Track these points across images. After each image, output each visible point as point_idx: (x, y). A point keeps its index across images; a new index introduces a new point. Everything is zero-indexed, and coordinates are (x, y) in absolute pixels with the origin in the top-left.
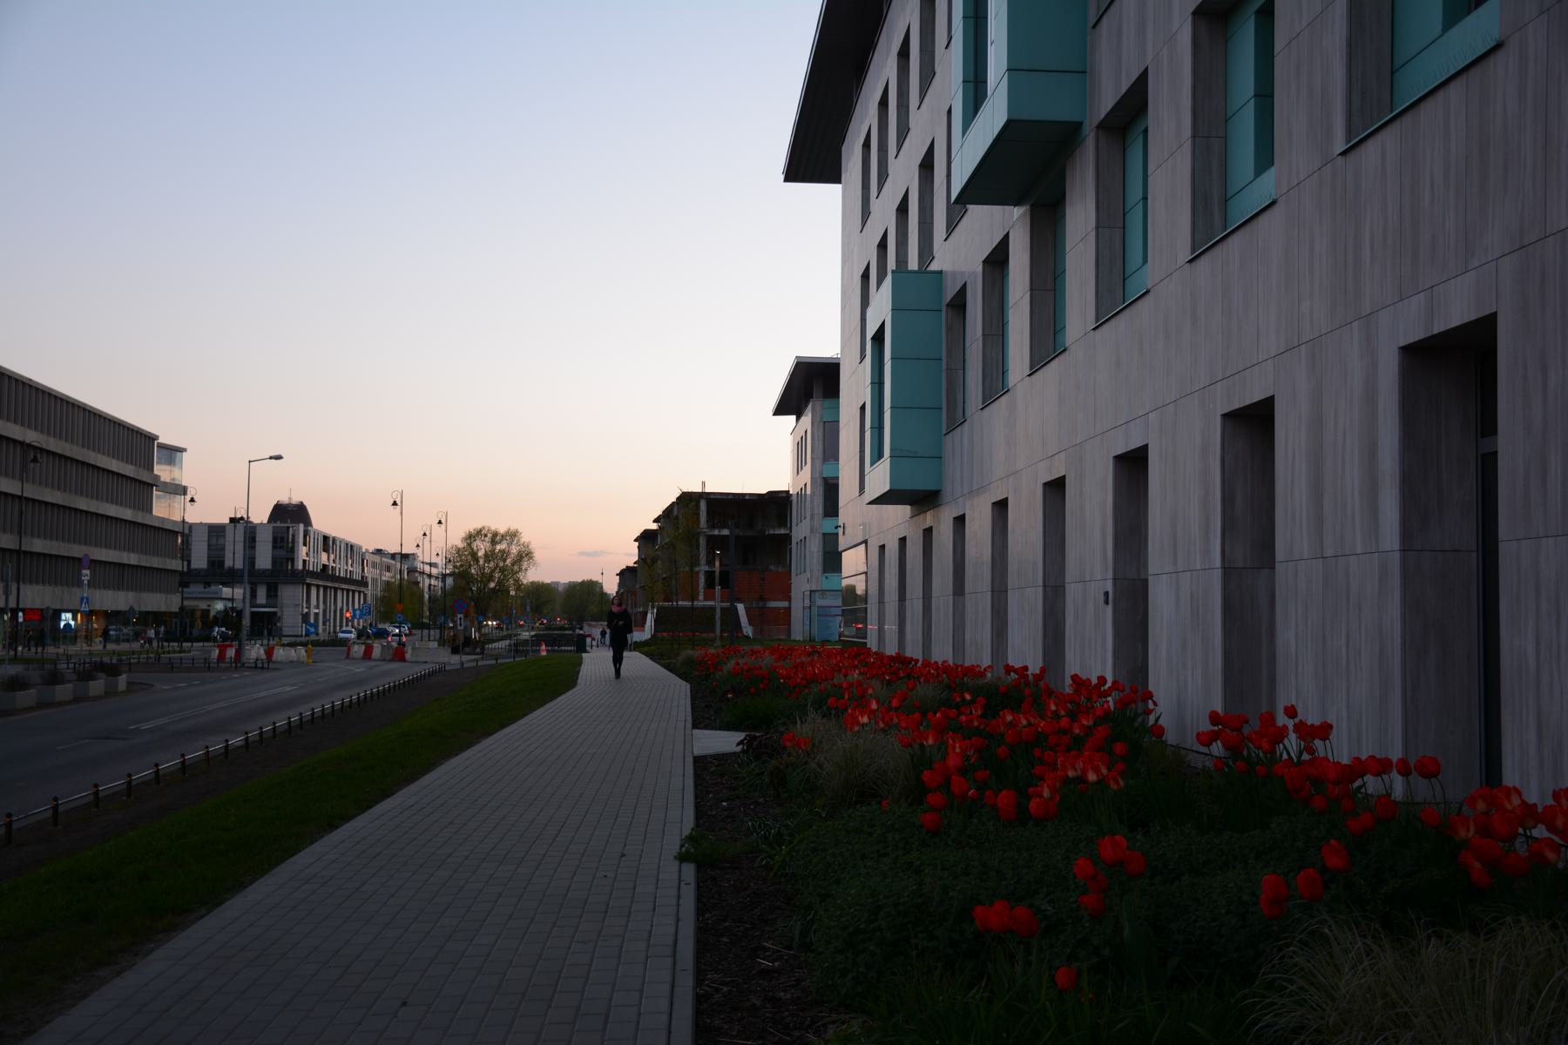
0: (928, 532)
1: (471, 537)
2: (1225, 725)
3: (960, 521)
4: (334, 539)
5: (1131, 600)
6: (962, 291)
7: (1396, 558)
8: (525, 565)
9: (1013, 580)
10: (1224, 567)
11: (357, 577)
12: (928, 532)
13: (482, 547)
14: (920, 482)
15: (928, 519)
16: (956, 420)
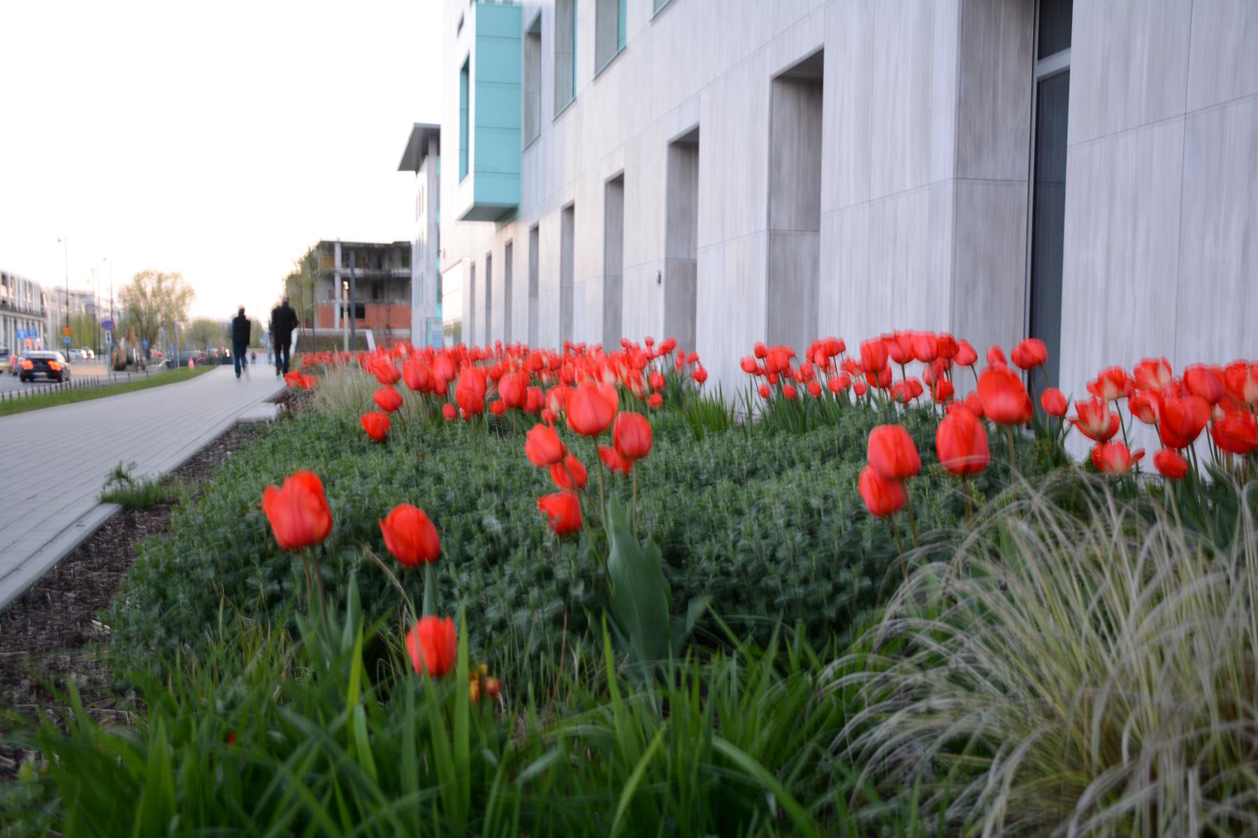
0: (509, 247)
1: (138, 279)
2: (771, 365)
3: (535, 230)
4: (12, 278)
5: (682, 279)
6: (538, 21)
7: (949, 188)
8: (188, 300)
9: (578, 277)
10: (769, 230)
11: (36, 307)
12: (509, 247)
13: (149, 286)
14: (503, 198)
15: (510, 232)
16: (532, 140)
